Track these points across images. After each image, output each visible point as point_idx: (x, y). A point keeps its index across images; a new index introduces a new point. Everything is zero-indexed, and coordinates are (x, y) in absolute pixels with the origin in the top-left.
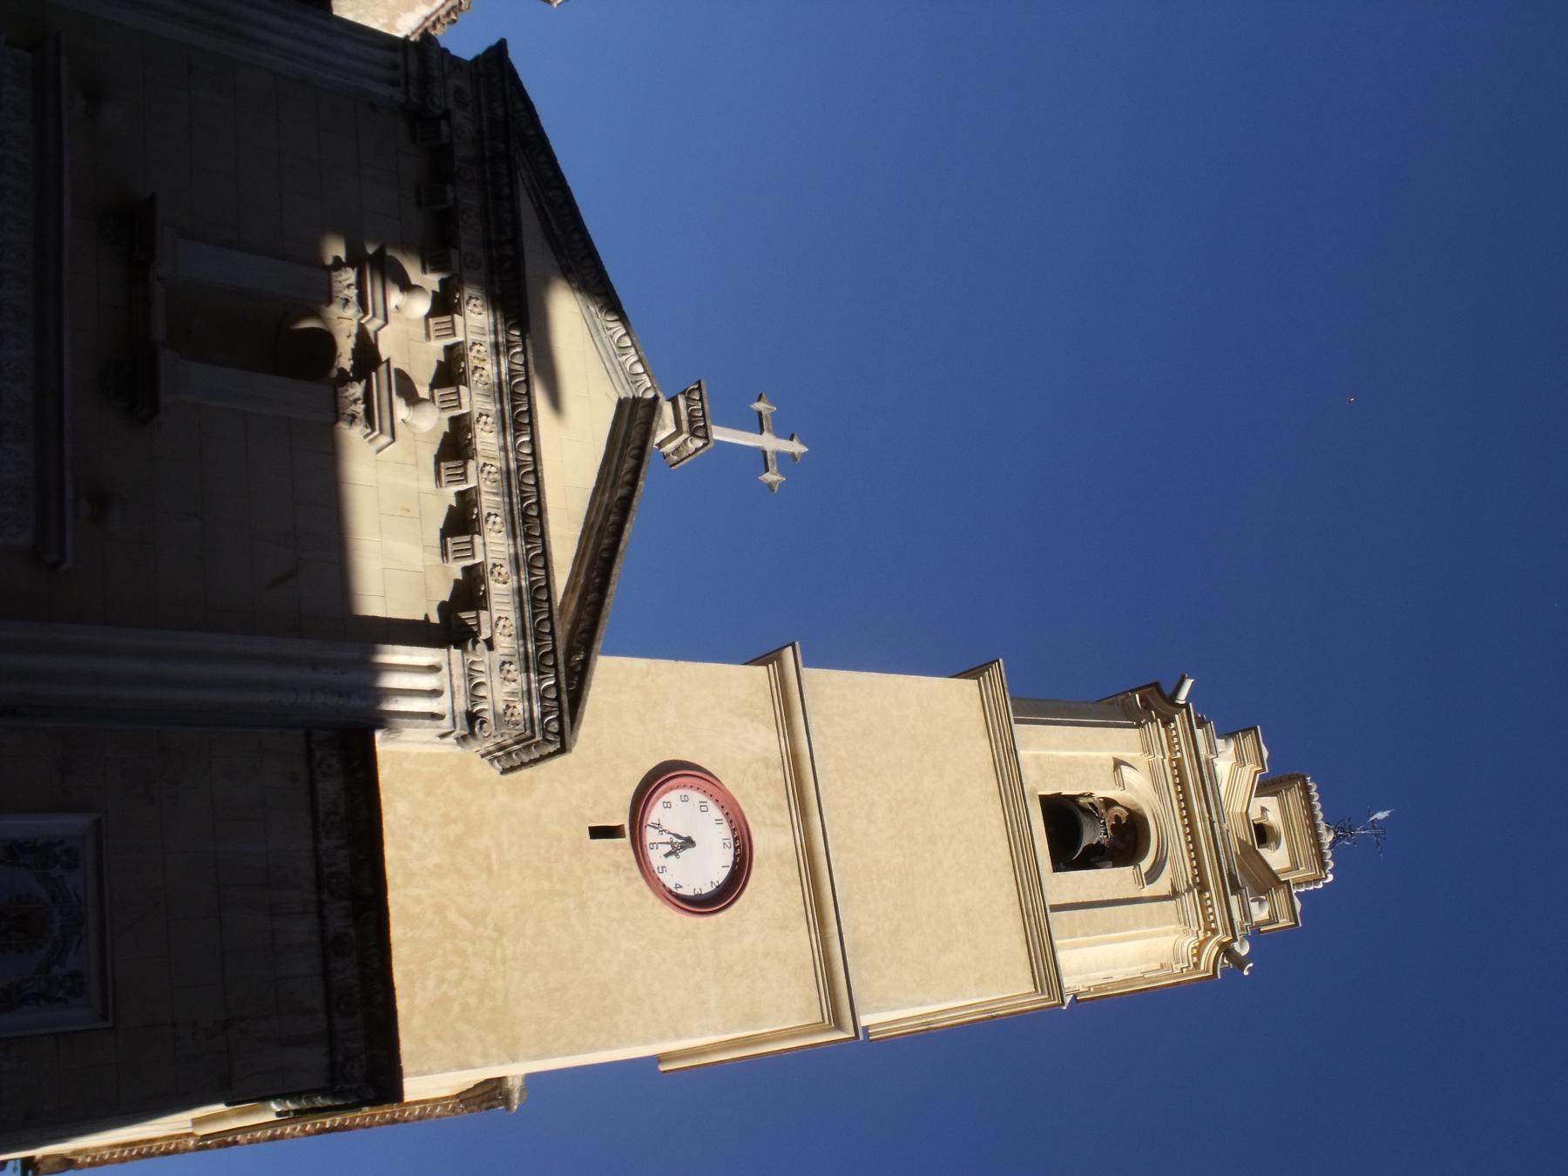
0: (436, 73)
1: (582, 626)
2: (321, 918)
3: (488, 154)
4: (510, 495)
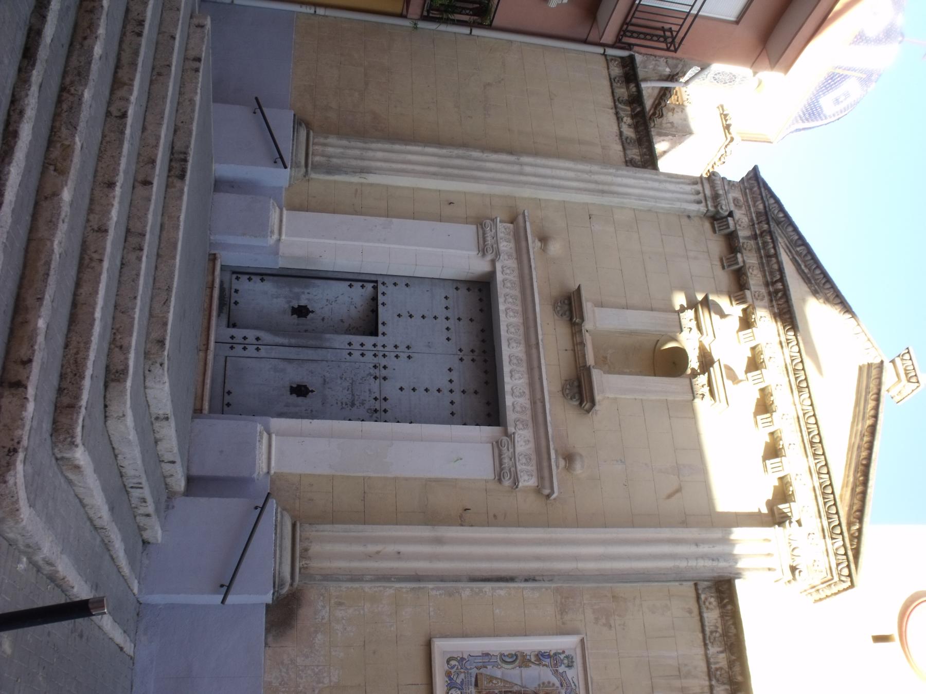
0: (721, 192)
1: (855, 508)
3: (758, 232)
4: (764, 271)
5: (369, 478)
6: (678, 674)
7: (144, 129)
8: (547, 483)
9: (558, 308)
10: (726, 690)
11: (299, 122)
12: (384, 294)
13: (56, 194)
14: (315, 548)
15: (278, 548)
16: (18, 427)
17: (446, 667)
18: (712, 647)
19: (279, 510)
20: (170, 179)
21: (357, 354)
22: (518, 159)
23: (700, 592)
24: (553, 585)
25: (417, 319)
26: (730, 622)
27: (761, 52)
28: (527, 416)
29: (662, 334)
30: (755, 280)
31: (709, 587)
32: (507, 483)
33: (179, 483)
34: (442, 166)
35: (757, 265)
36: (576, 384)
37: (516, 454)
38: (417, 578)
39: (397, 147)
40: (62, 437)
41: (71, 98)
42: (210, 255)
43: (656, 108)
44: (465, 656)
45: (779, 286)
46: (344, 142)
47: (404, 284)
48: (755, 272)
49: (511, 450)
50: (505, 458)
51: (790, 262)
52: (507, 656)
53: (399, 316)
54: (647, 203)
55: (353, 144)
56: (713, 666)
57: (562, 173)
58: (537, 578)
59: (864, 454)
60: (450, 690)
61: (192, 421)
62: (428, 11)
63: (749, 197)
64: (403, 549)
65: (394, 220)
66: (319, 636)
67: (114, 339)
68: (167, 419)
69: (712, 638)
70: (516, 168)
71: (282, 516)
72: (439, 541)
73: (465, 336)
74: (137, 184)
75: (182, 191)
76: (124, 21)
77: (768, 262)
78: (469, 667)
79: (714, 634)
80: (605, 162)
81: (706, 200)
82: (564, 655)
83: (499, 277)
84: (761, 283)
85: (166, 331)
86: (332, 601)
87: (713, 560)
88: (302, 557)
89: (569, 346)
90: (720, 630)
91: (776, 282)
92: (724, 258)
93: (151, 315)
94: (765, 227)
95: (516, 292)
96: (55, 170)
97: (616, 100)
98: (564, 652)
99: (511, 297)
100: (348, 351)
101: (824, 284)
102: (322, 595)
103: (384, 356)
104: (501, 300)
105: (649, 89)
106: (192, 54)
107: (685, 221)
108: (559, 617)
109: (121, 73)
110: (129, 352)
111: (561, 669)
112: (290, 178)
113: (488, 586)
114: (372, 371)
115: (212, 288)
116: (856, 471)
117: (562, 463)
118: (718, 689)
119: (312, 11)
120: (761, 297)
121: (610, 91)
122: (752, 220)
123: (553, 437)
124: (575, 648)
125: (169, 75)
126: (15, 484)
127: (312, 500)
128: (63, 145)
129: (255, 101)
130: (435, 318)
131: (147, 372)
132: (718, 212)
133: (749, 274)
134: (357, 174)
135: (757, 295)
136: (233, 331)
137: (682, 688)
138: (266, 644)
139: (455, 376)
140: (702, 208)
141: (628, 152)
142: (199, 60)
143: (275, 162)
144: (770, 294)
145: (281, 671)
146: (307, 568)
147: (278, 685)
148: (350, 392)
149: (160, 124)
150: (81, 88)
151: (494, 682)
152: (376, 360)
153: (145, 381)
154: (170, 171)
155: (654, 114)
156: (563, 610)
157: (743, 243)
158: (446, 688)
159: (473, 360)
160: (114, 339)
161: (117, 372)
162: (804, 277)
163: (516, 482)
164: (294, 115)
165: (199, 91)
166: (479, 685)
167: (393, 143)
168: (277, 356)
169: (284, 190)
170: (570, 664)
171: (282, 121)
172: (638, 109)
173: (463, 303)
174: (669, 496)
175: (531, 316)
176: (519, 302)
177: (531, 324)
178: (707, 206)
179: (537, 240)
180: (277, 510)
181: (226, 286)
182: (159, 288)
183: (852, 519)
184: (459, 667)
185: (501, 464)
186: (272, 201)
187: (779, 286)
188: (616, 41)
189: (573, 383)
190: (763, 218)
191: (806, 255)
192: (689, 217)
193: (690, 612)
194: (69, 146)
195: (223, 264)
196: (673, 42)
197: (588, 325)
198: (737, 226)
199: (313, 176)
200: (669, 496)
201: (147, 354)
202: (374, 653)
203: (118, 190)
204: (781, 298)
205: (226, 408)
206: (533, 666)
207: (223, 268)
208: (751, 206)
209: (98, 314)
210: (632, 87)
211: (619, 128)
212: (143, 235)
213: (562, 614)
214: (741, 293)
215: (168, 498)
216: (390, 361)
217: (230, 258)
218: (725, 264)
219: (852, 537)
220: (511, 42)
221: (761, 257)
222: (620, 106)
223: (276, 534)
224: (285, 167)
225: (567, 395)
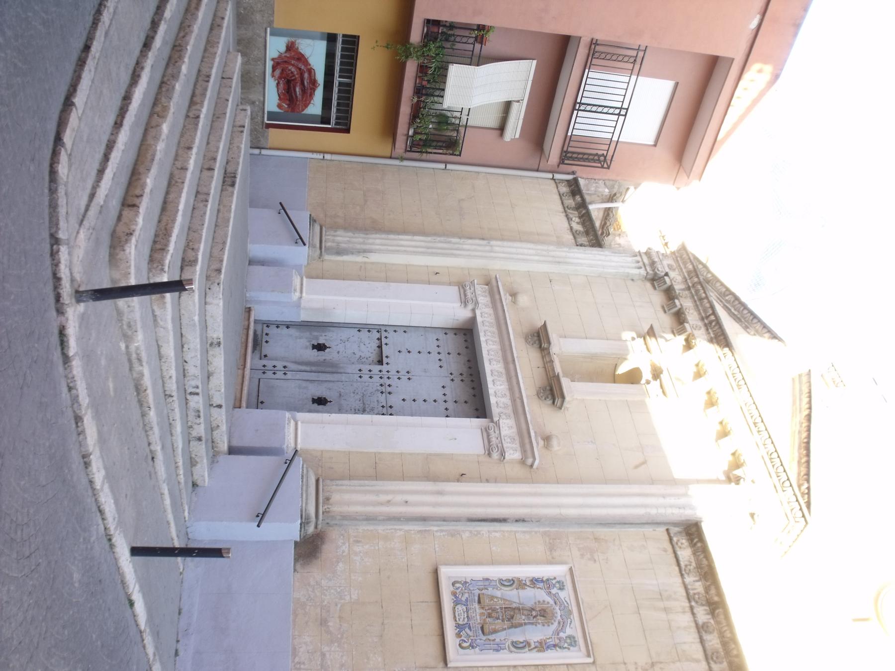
0: (656, 260)
1: (802, 474)
2: (693, 614)
3: (690, 285)
4: (699, 310)
5: (380, 453)
6: (660, 597)
7: (208, 143)
8: (529, 453)
9: (529, 340)
10: (706, 610)
11: (312, 221)
12: (386, 337)
13: (158, 126)
14: (336, 497)
15: (304, 492)
16: (133, 224)
17: (452, 589)
18: (689, 577)
19: (305, 466)
20: (224, 187)
21: (366, 377)
22: (489, 243)
23: (672, 535)
24: (542, 530)
25: (414, 354)
26: (702, 556)
27: (679, 169)
28: (510, 411)
29: (618, 356)
30: (692, 317)
31: (680, 532)
32: (496, 455)
33: (225, 447)
34: (428, 248)
35: (693, 307)
36: (548, 388)
37: (502, 436)
38: (424, 519)
39: (392, 236)
40: (155, 265)
41: (167, 86)
42: (246, 308)
43: (603, 228)
44: (468, 580)
45: (712, 318)
46: (350, 234)
47: (403, 331)
48: (691, 311)
49: (497, 432)
50: (492, 438)
51: (722, 309)
52: (505, 580)
53: (399, 352)
54: (596, 269)
55: (356, 235)
56: (691, 592)
57: (526, 251)
58: (526, 520)
59: (805, 435)
60: (456, 605)
61: (233, 410)
62: (411, 148)
63: (680, 262)
64: (411, 498)
65: (392, 284)
66: (341, 565)
67: (188, 245)
68: (219, 344)
69: (687, 570)
70: (488, 248)
71: (307, 471)
72: (440, 493)
73: (455, 364)
74: (203, 170)
75: (233, 193)
76: (197, 76)
77: (701, 304)
78: (472, 589)
79: (689, 567)
80: (560, 243)
81: (645, 266)
82: (556, 581)
83: (479, 319)
84: (698, 319)
85: (222, 265)
86: (351, 540)
87: (680, 508)
88: (324, 503)
89: (540, 364)
90: (694, 564)
91: (710, 315)
92: (665, 306)
93: (211, 256)
94: (696, 280)
95: (495, 329)
96: (158, 116)
97: (565, 209)
98: (555, 578)
99: (490, 332)
100: (359, 375)
101: (752, 320)
102: (342, 535)
103: (389, 378)
104: (482, 334)
105: (596, 209)
106: (238, 123)
107: (629, 283)
108: (548, 553)
109: (195, 99)
110: (199, 252)
111: (554, 591)
112: (308, 256)
113: (484, 528)
114: (379, 388)
115: (248, 329)
116: (800, 448)
117: (541, 443)
118: (698, 610)
119: (321, 157)
120: (698, 328)
121: (560, 202)
122: (685, 278)
123: (531, 421)
124: (565, 576)
125: (225, 118)
126: (130, 253)
127: (332, 468)
128: (162, 105)
129: (279, 205)
130: (429, 353)
131: (208, 290)
132: (655, 274)
133: (686, 313)
134: (361, 254)
135: (694, 326)
136: (264, 362)
137: (665, 608)
138: (295, 570)
139: (447, 391)
140: (643, 272)
141: (579, 240)
142: (244, 127)
143: (296, 243)
144: (705, 325)
145: (308, 590)
146: (329, 512)
147: (305, 600)
148: (361, 402)
149: (219, 141)
150: (174, 82)
151: (495, 600)
152: (382, 381)
153: (205, 297)
154: (224, 182)
155: (602, 233)
156: (552, 548)
157: (679, 293)
158: (453, 604)
159: (462, 380)
160: (188, 245)
161: (190, 261)
162: (735, 318)
163: (502, 454)
164: (310, 215)
165: (243, 142)
166: (482, 602)
167: (388, 234)
168: (301, 378)
169: (303, 266)
170: (561, 587)
171: (302, 220)
172: (584, 212)
173: (451, 343)
174: (636, 467)
175: (507, 343)
176: (497, 336)
177: (508, 348)
178: (646, 270)
179: (508, 295)
180: (303, 465)
181: (259, 333)
182: (217, 242)
183: (801, 482)
184: (463, 589)
185: (489, 442)
186: (294, 271)
187: (712, 318)
188: (560, 162)
189: (546, 389)
190: (693, 274)
191: (734, 301)
192: (633, 280)
193: (665, 550)
194: (166, 106)
195: (256, 319)
196: (605, 160)
197: (554, 349)
198: (673, 282)
199: (327, 257)
200: (636, 467)
201: (208, 278)
202: (389, 577)
203: (195, 150)
204: (715, 326)
205: (260, 404)
206: (528, 588)
207: (256, 321)
208: (683, 268)
209: (181, 207)
210: (578, 198)
211: (570, 224)
212: (208, 194)
213: (551, 551)
214: (682, 326)
215: (214, 456)
216: (394, 381)
217: (261, 312)
218: (666, 309)
219: (803, 494)
220: (478, 173)
221: (695, 301)
222: (569, 211)
223: (302, 481)
224: (305, 244)
225: (542, 397)
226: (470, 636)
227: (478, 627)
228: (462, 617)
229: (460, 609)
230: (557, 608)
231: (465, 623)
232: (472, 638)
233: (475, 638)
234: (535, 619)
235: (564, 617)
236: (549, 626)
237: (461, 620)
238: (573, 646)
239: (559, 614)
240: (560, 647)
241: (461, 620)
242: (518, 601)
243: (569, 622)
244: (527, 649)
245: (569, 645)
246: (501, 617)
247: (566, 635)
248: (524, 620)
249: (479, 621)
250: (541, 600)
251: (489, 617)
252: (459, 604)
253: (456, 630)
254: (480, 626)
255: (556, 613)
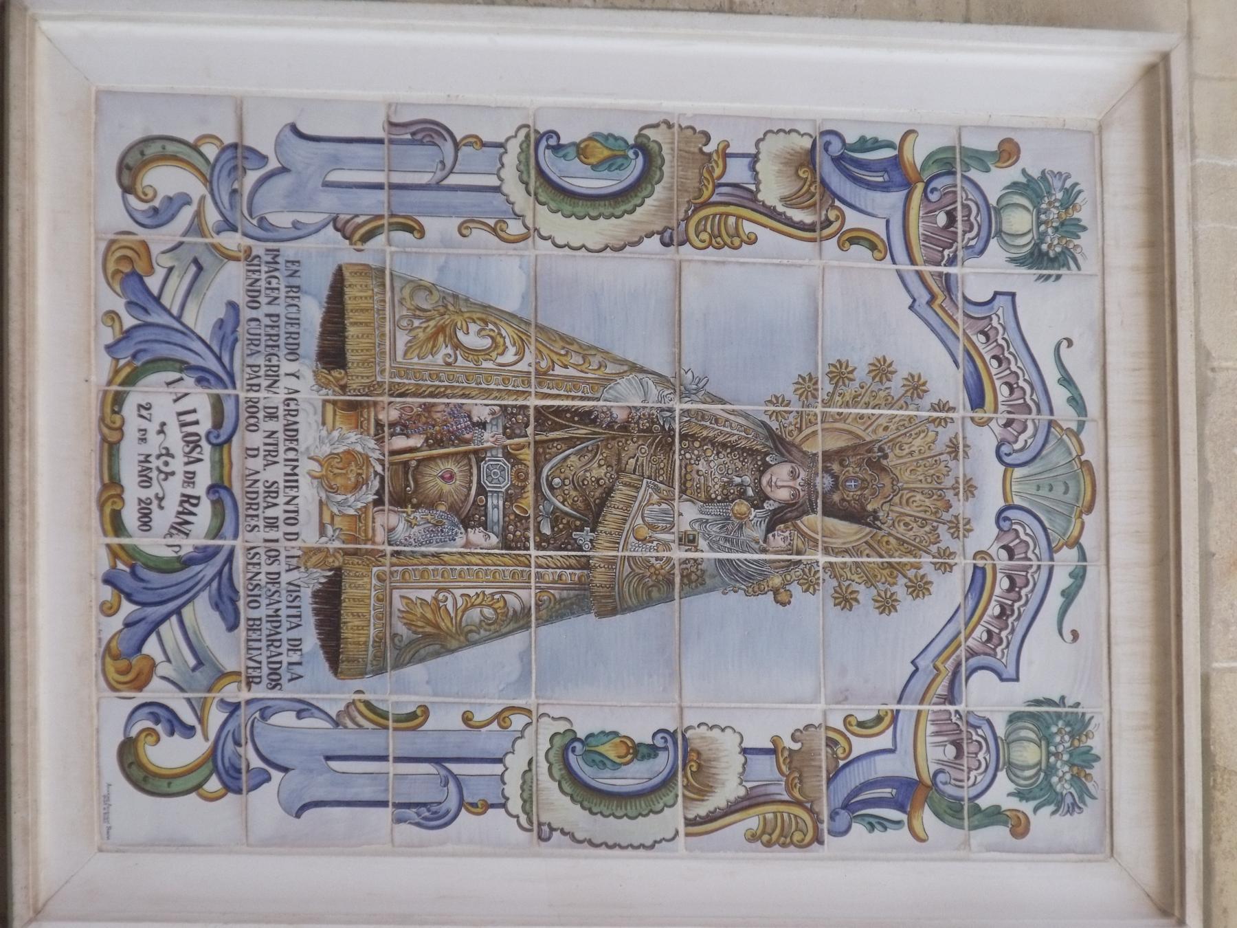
44: (261, 138)
52: (581, 150)
78: (282, 220)
82: (1012, 174)
98: (1008, 152)
151: (472, 339)
158: (106, 363)
170: (1052, 243)
184: (212, 216)
206: (767, 237)
226: (222, 675)
227: (294, 587)
228: (174, 489)
229: (164, 408)
230: (984, 441)
231: (187, 546)
232: (233, 692)
233: (259, 692)
234: (778, 539)
235: (1027, 528)
236: (887, 605)
237: (163, 518)
238: (1057, 802)
239: (992, 500)
240: (952, 812)
241: (163, 518)
242: (658, 360)
243: (1061, 580)
244: (674, 817)
245: (1021, 795)
246: (495, 508)
247: (1017, 696)
248: (688, 541)
249: (309, 536)
250: (860, 362)
251: (400, 501)
252: (159, 364)
253: (108, 610)
254: (311, 581)
255: (971, 489)
